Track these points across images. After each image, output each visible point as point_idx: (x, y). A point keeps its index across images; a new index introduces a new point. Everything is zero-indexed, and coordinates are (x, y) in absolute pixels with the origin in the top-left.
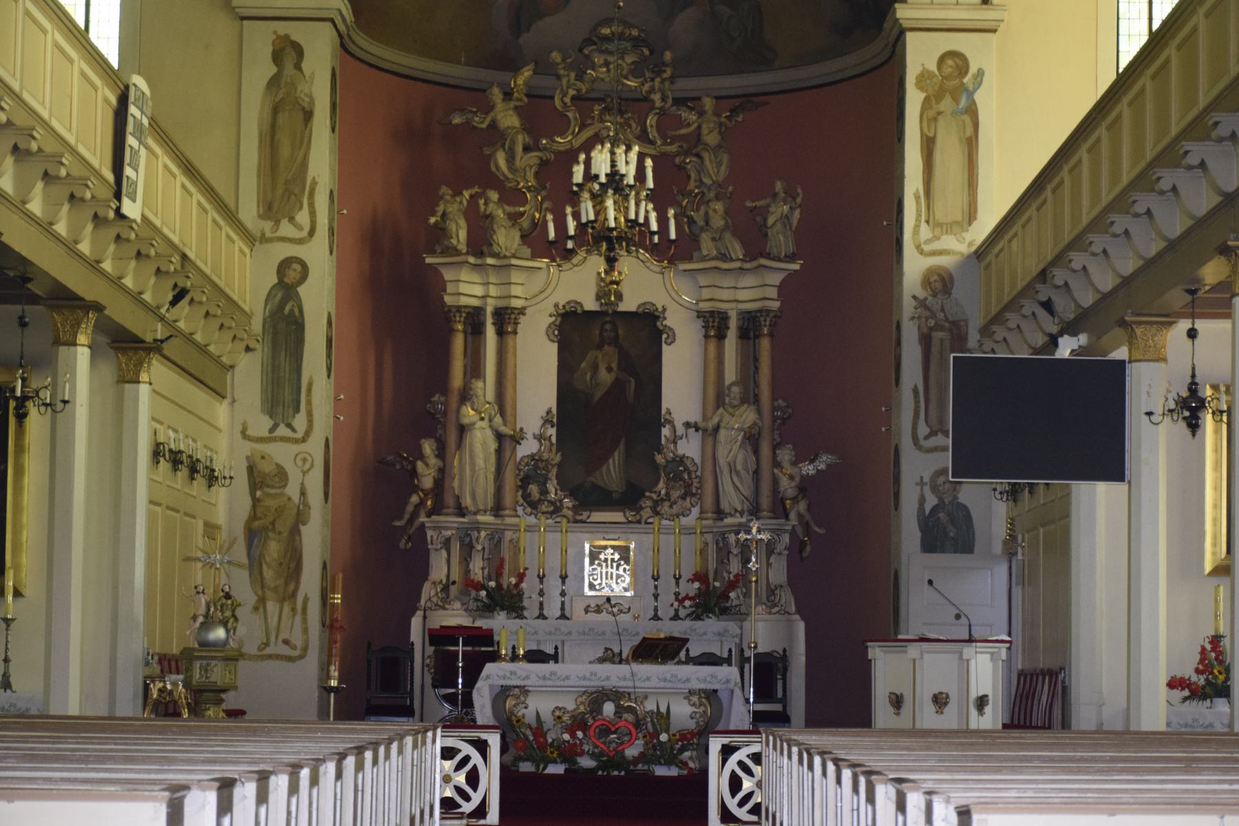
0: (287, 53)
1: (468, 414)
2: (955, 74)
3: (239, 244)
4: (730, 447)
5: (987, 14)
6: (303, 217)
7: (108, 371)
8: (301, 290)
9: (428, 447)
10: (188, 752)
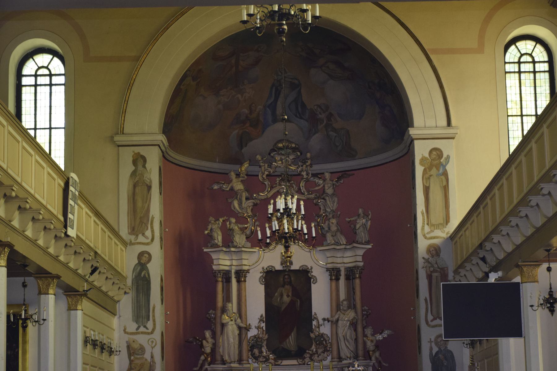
0: (139, 160)
1: (225, 318)
2: (437, 159)
3: (120, 246)
4: (344, 328)
5: (450, 131)
6: (148, 233)
7: (63, 305)
9: (208, 334)
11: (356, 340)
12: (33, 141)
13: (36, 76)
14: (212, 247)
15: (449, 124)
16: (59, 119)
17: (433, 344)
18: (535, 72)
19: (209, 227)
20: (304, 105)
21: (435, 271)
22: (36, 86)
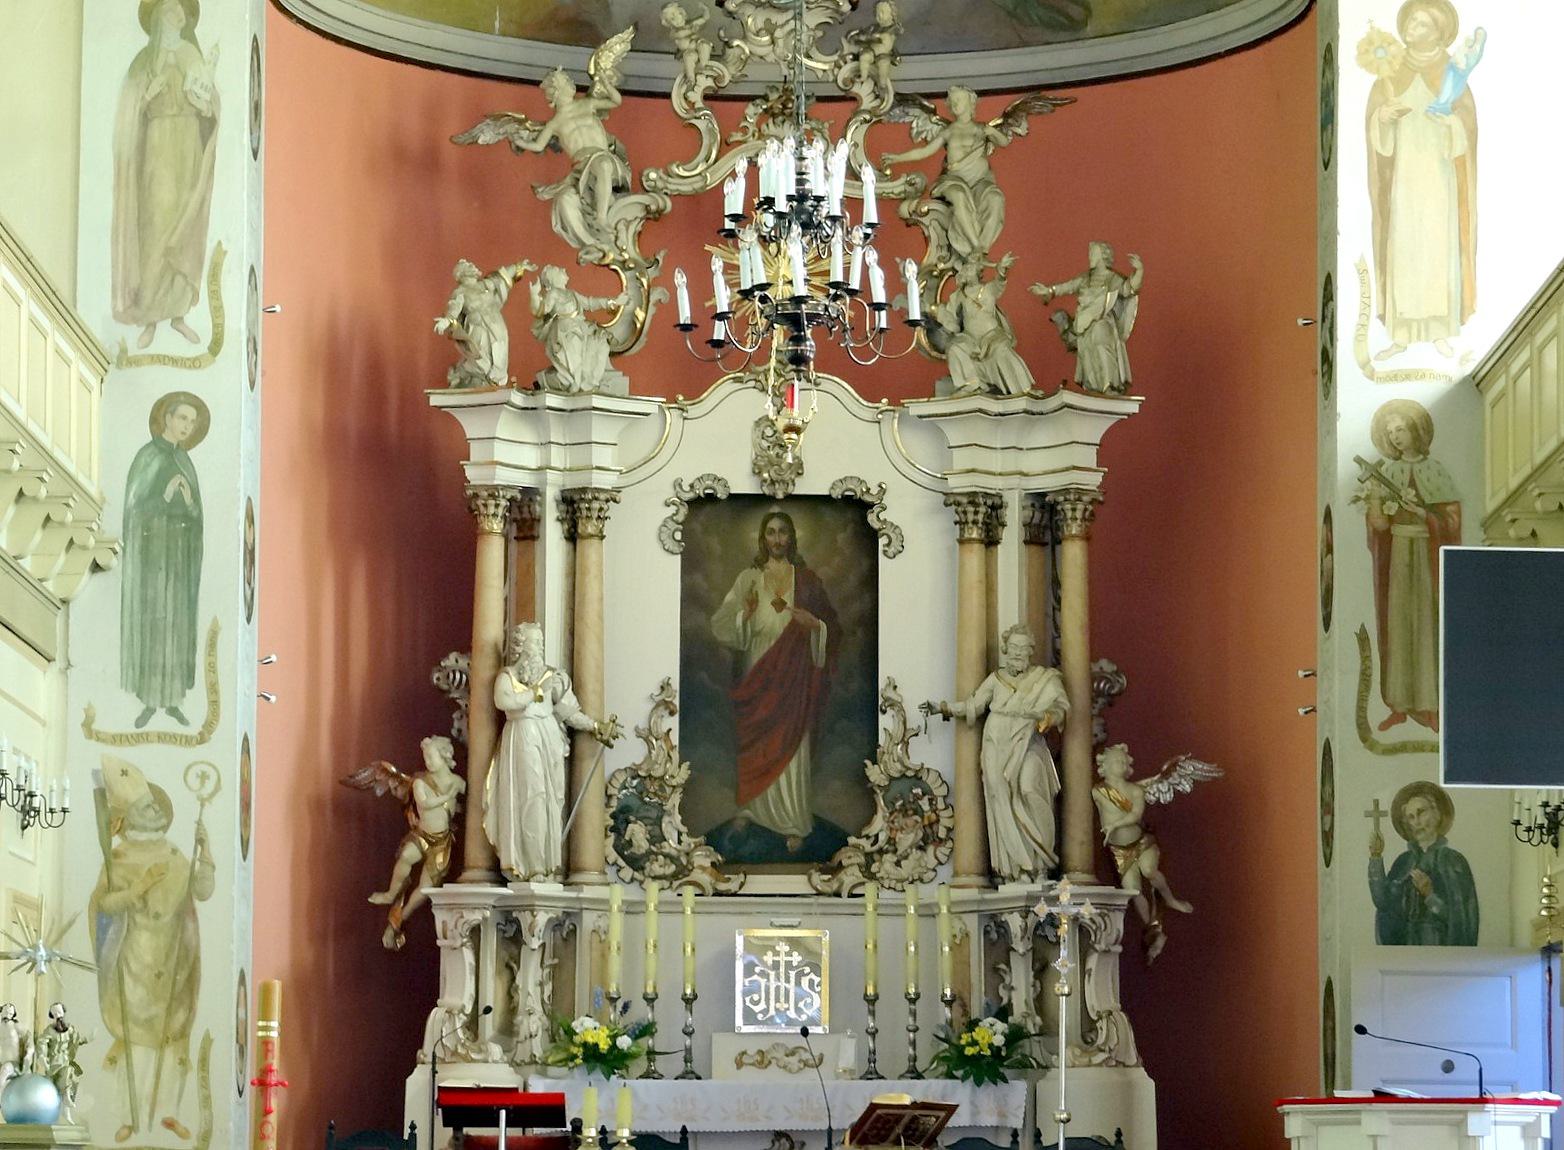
1: (511, 691)
4: (1009, 751)
6: (199, 317)
9: (437, 752)
17: (1387, 823)
21: (1404, 517)
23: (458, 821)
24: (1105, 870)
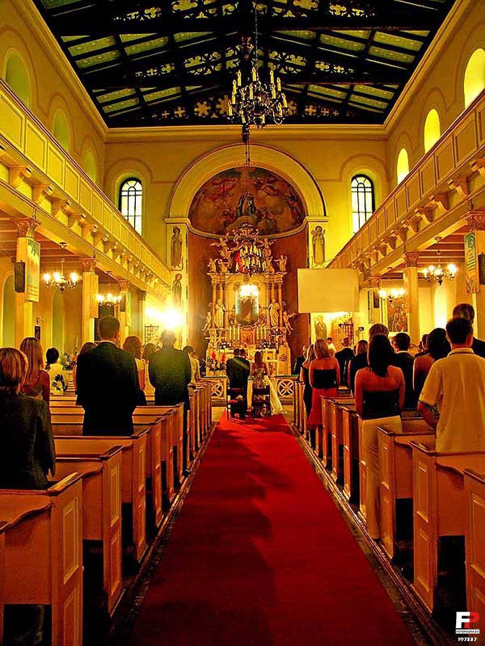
0: (176, 230)
1: (217, 307)
2: (319, 231)
3: (167, 271)
4: (273, 312)
5: (326, 218)
6: (181, 265)
7: (136, 298)
8: (181, 281)
9: (209, 314)
10: (303, 420)
11: (279, 318)
12: (127, 222)
13: (358, 187)
14: (211, 272)
15: (325, 215)
16: (139, 212)
18: (365, 192)
19: (210, 263)
20: (255, 208)
22: (135, 195)
23: (211, 321)
24: (284, 325)
